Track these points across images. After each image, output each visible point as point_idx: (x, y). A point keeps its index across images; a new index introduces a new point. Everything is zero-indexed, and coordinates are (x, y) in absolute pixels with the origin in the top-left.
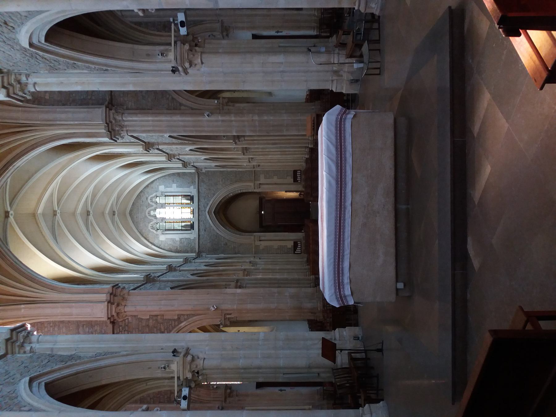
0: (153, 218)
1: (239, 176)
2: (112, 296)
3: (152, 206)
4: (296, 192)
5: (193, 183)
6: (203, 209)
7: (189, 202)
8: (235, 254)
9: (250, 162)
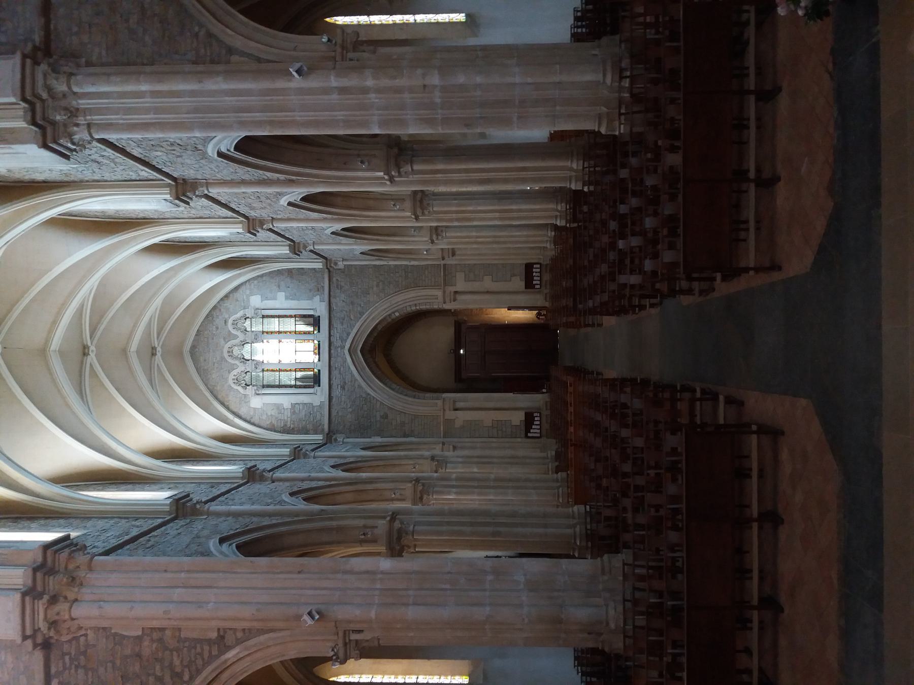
0: (237, 362)
1: (413, 277)
2: (39, 575)
3: (236, 337)
4: (531, 308)
5: (319, 290)
6: (339, 343)
7: (310, 329)
8: (405, 436)
9: (432, 242)
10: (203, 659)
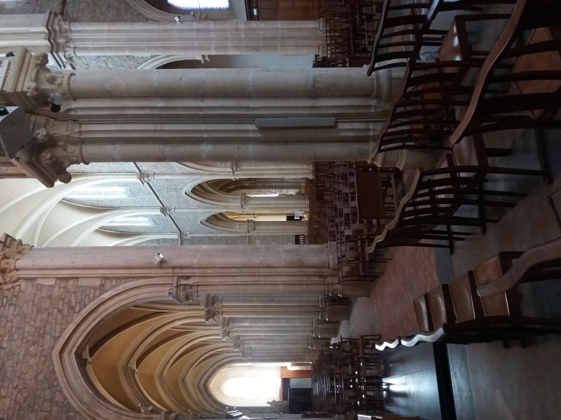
10: (89, 298)
